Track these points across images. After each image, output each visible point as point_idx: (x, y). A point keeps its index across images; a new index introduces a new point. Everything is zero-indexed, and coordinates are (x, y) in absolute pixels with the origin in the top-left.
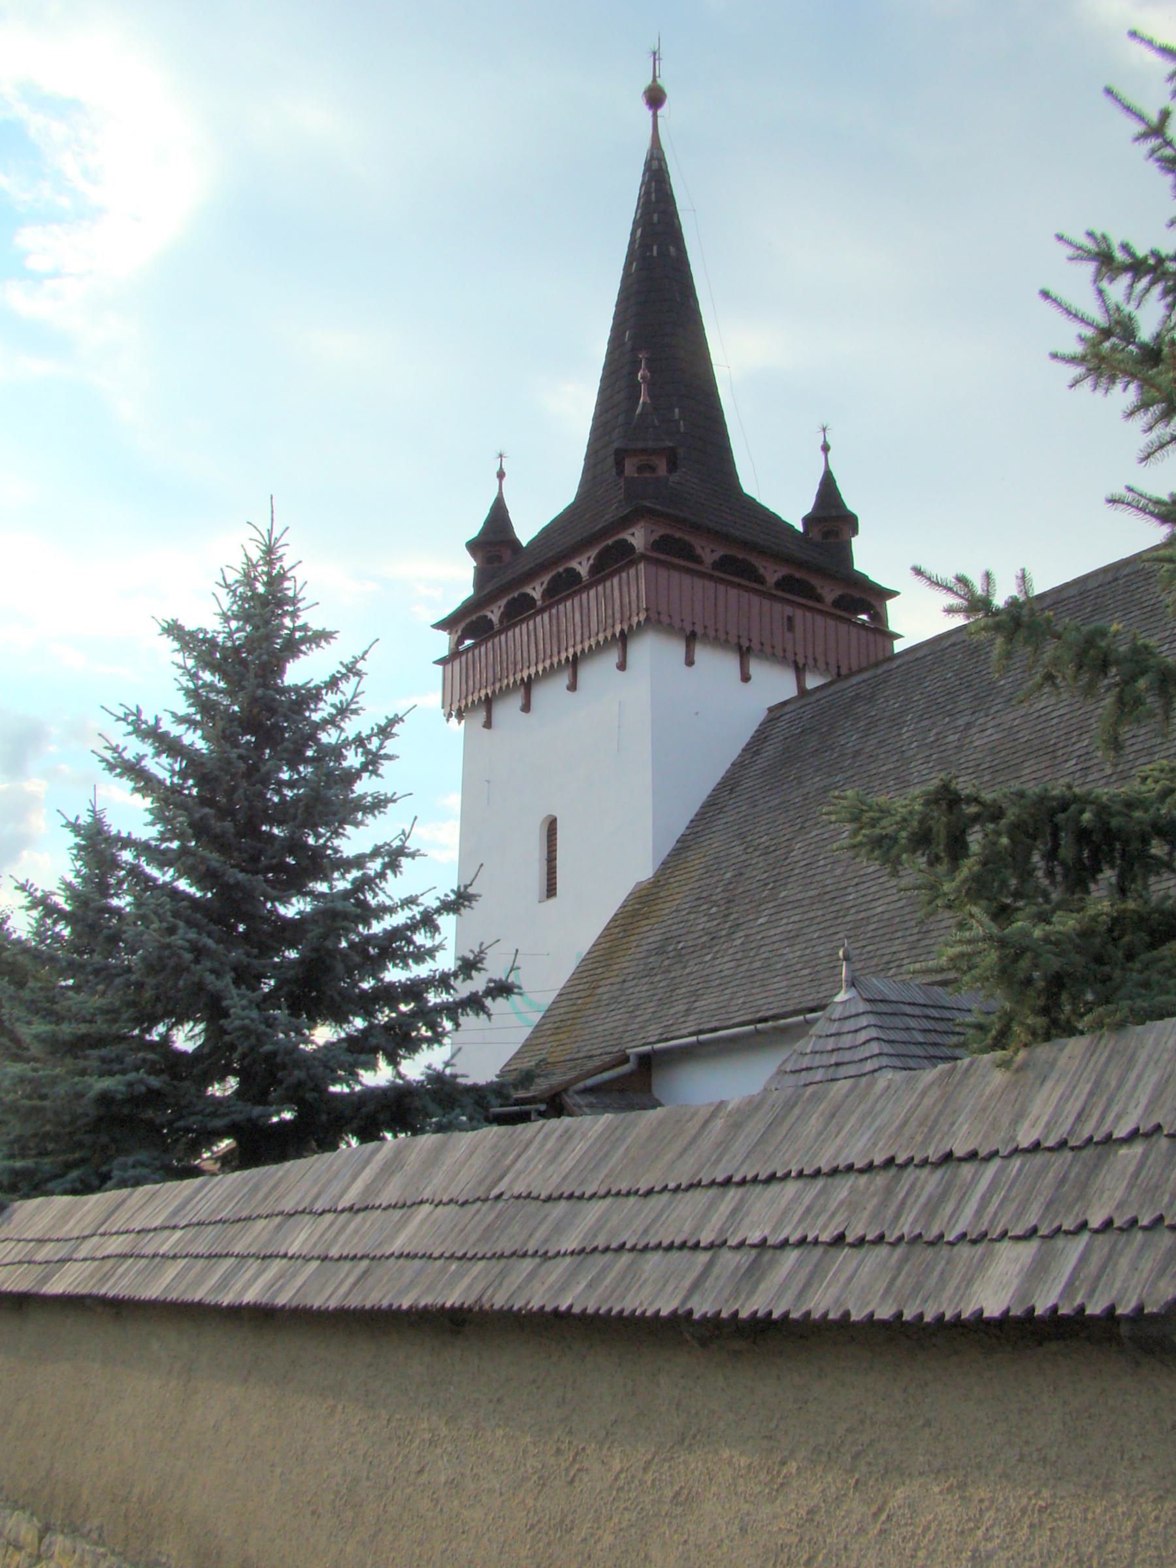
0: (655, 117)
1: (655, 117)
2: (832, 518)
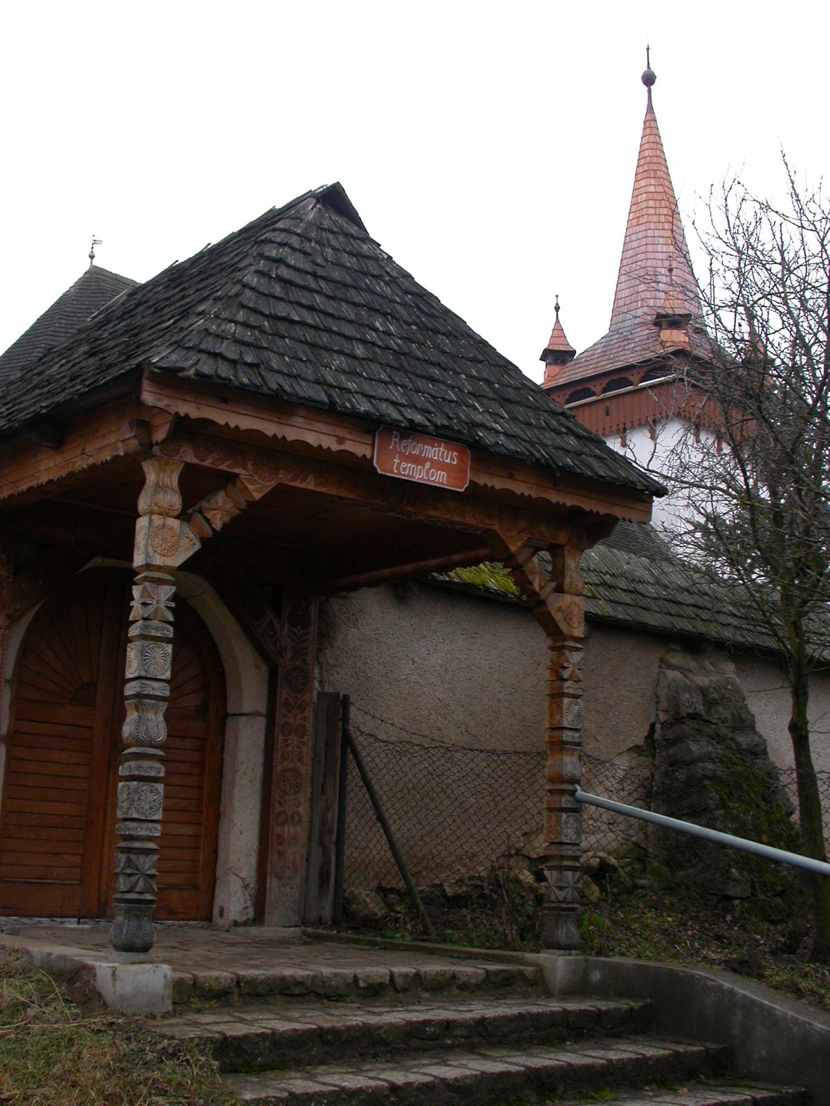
0: (649, 91)
1: (649, 91)
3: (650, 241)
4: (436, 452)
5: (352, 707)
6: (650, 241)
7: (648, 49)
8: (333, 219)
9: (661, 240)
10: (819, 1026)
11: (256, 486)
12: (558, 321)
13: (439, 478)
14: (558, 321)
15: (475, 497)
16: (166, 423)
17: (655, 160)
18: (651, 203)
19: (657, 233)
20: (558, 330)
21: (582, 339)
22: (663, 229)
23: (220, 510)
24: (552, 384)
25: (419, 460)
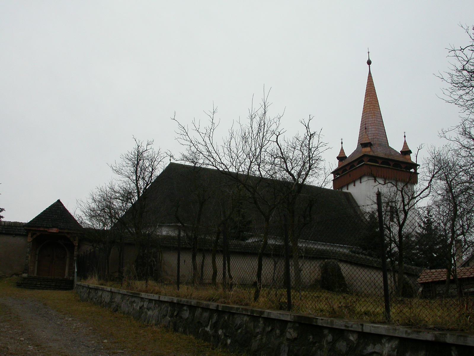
0: (369, 67)
1: (369, 67)
2: (406, 152)
3: (367, 118)
4: (54, 229)
5: (372, 271)
6: (367, 118)
7: (369, 52)
8: (59, 203)
9: (371, 117)
10: (205, 302)
11: (38, 234)
12: (342, 147)
13: (55, 231)
14: (342, 147)
15: (59, 232)
16: (416, 162)
17: (370, 90)
18: (368, 105)
19: (369, 115)
20: (342, 150)
21: (348, 153)
22: (371, 113)
23: (35, 236)
24: (340, 167)
25: (53, 230)
